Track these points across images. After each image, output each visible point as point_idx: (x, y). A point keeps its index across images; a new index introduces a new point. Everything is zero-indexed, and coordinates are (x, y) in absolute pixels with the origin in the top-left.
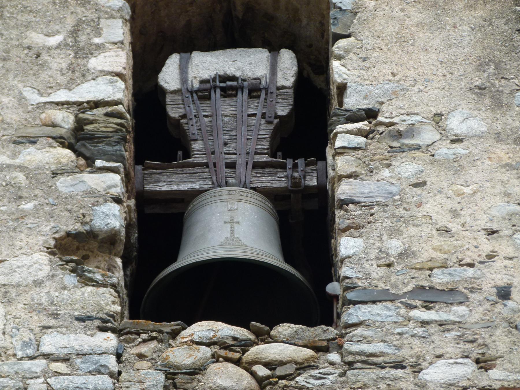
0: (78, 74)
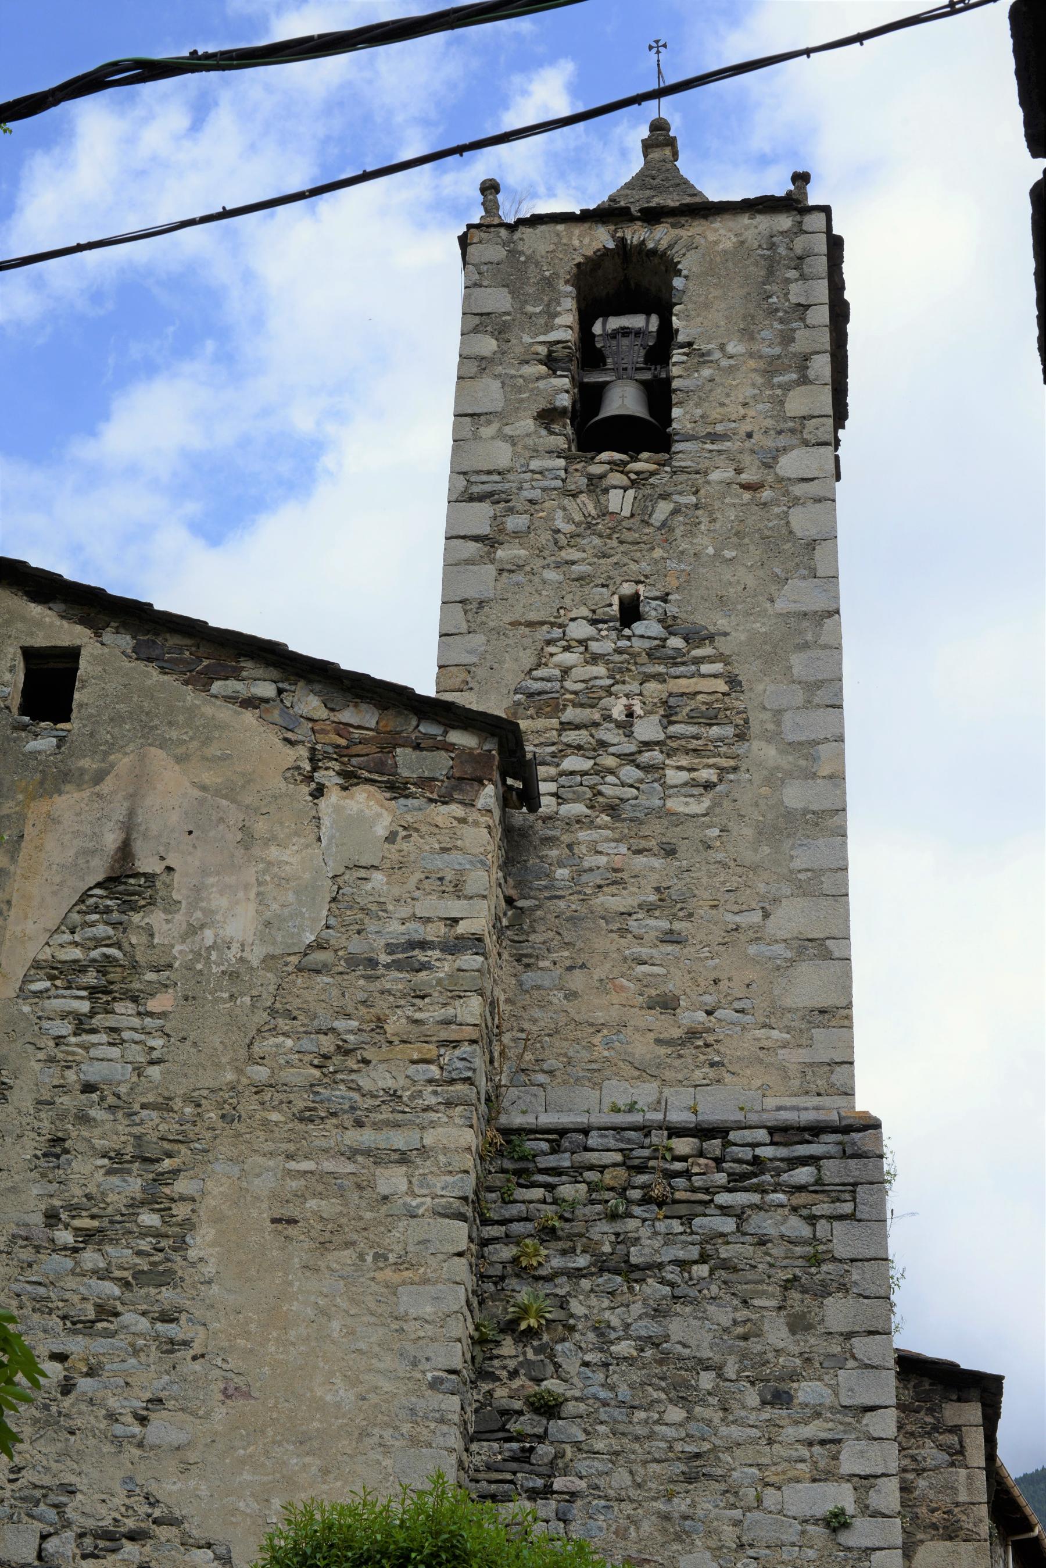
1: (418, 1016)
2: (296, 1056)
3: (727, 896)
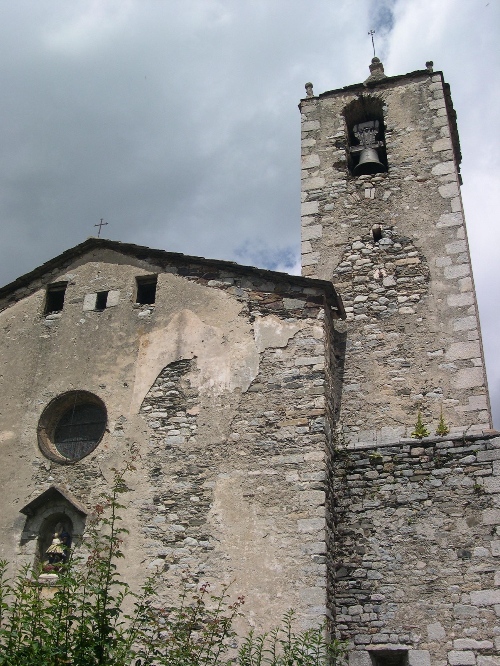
0: (335, 132)
1: (299, 407)
2: (250, 428)
3: (427, 345)
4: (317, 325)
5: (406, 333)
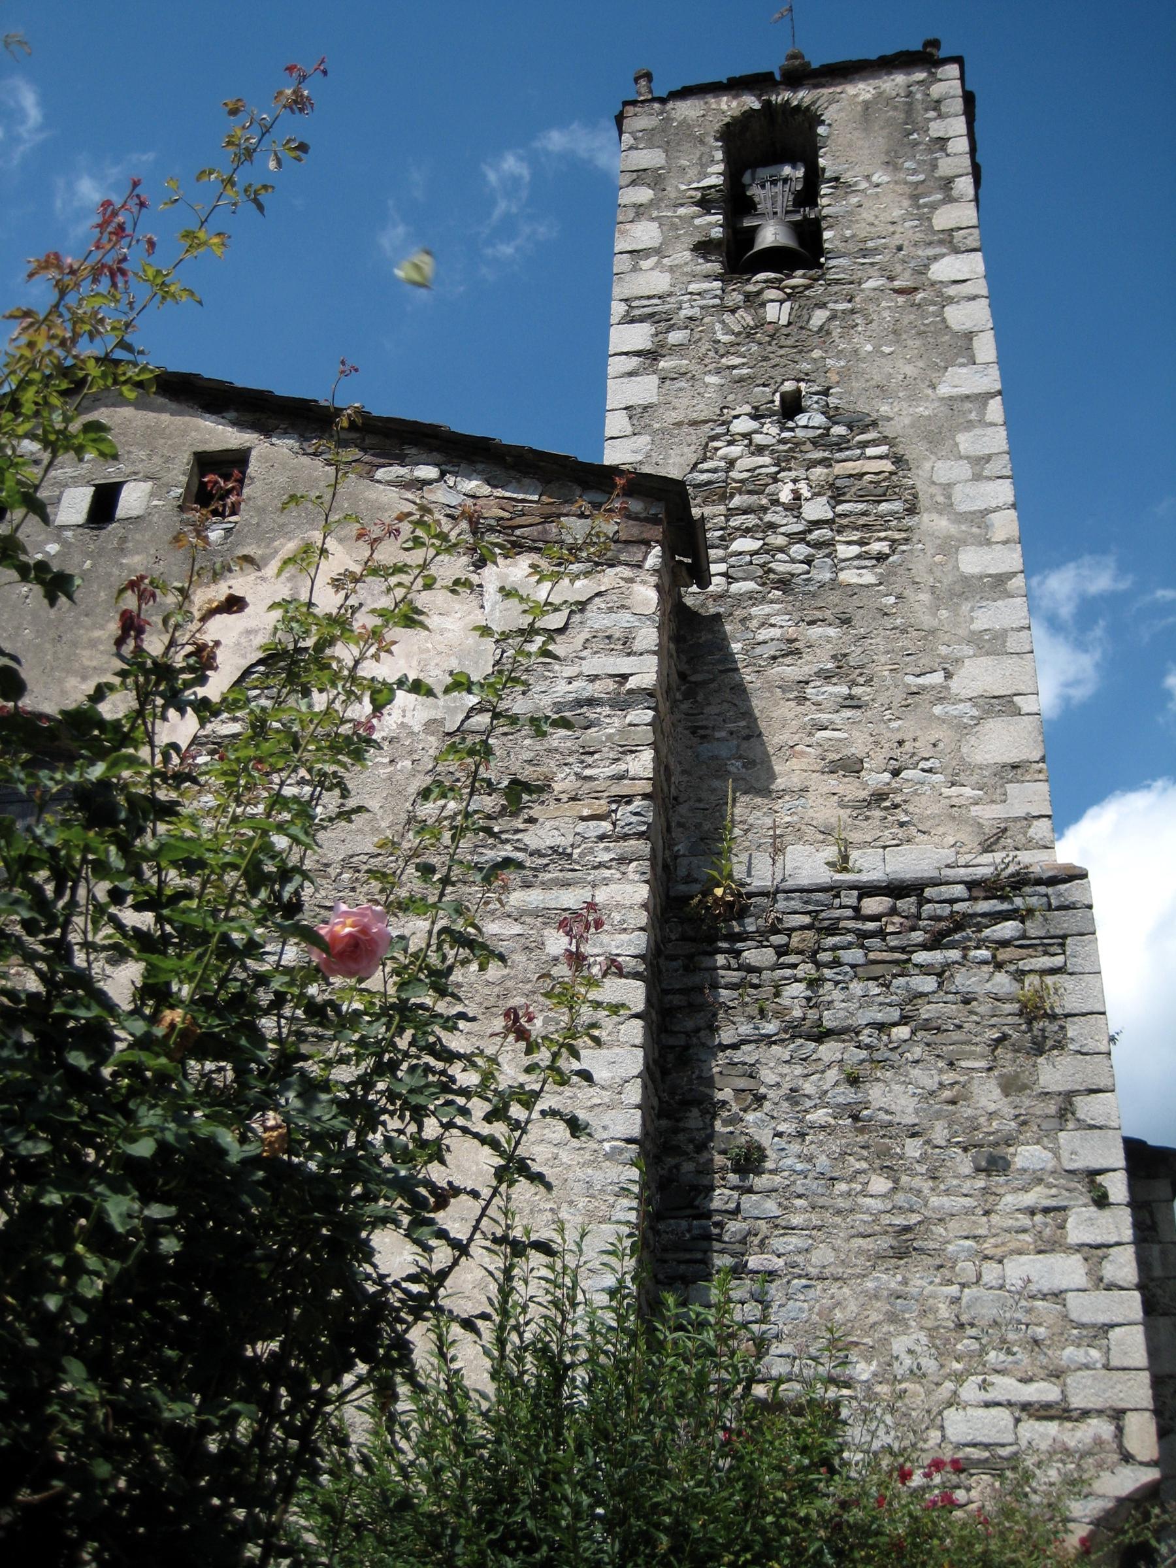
1: (587, 772)
3: (907, 659)
4: (643, 582)
5: (854, 627)
